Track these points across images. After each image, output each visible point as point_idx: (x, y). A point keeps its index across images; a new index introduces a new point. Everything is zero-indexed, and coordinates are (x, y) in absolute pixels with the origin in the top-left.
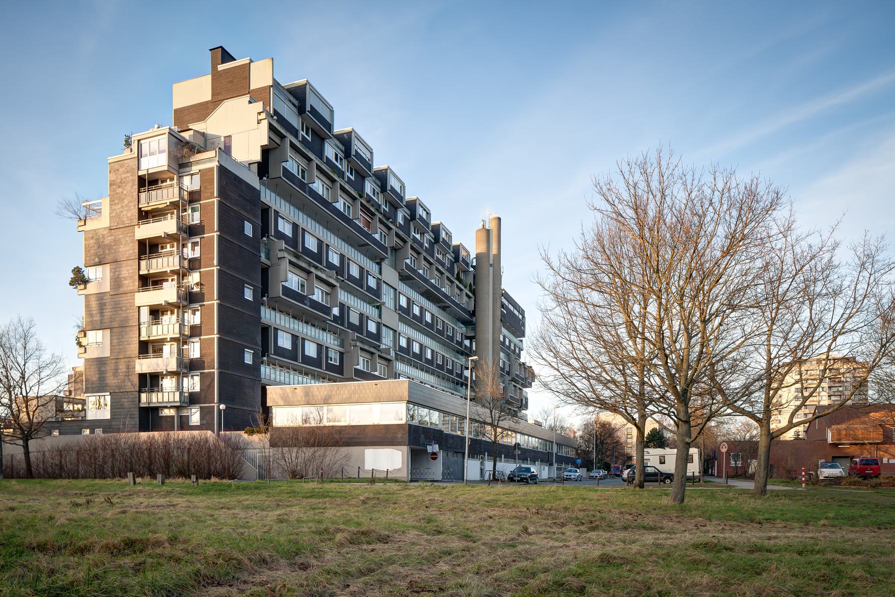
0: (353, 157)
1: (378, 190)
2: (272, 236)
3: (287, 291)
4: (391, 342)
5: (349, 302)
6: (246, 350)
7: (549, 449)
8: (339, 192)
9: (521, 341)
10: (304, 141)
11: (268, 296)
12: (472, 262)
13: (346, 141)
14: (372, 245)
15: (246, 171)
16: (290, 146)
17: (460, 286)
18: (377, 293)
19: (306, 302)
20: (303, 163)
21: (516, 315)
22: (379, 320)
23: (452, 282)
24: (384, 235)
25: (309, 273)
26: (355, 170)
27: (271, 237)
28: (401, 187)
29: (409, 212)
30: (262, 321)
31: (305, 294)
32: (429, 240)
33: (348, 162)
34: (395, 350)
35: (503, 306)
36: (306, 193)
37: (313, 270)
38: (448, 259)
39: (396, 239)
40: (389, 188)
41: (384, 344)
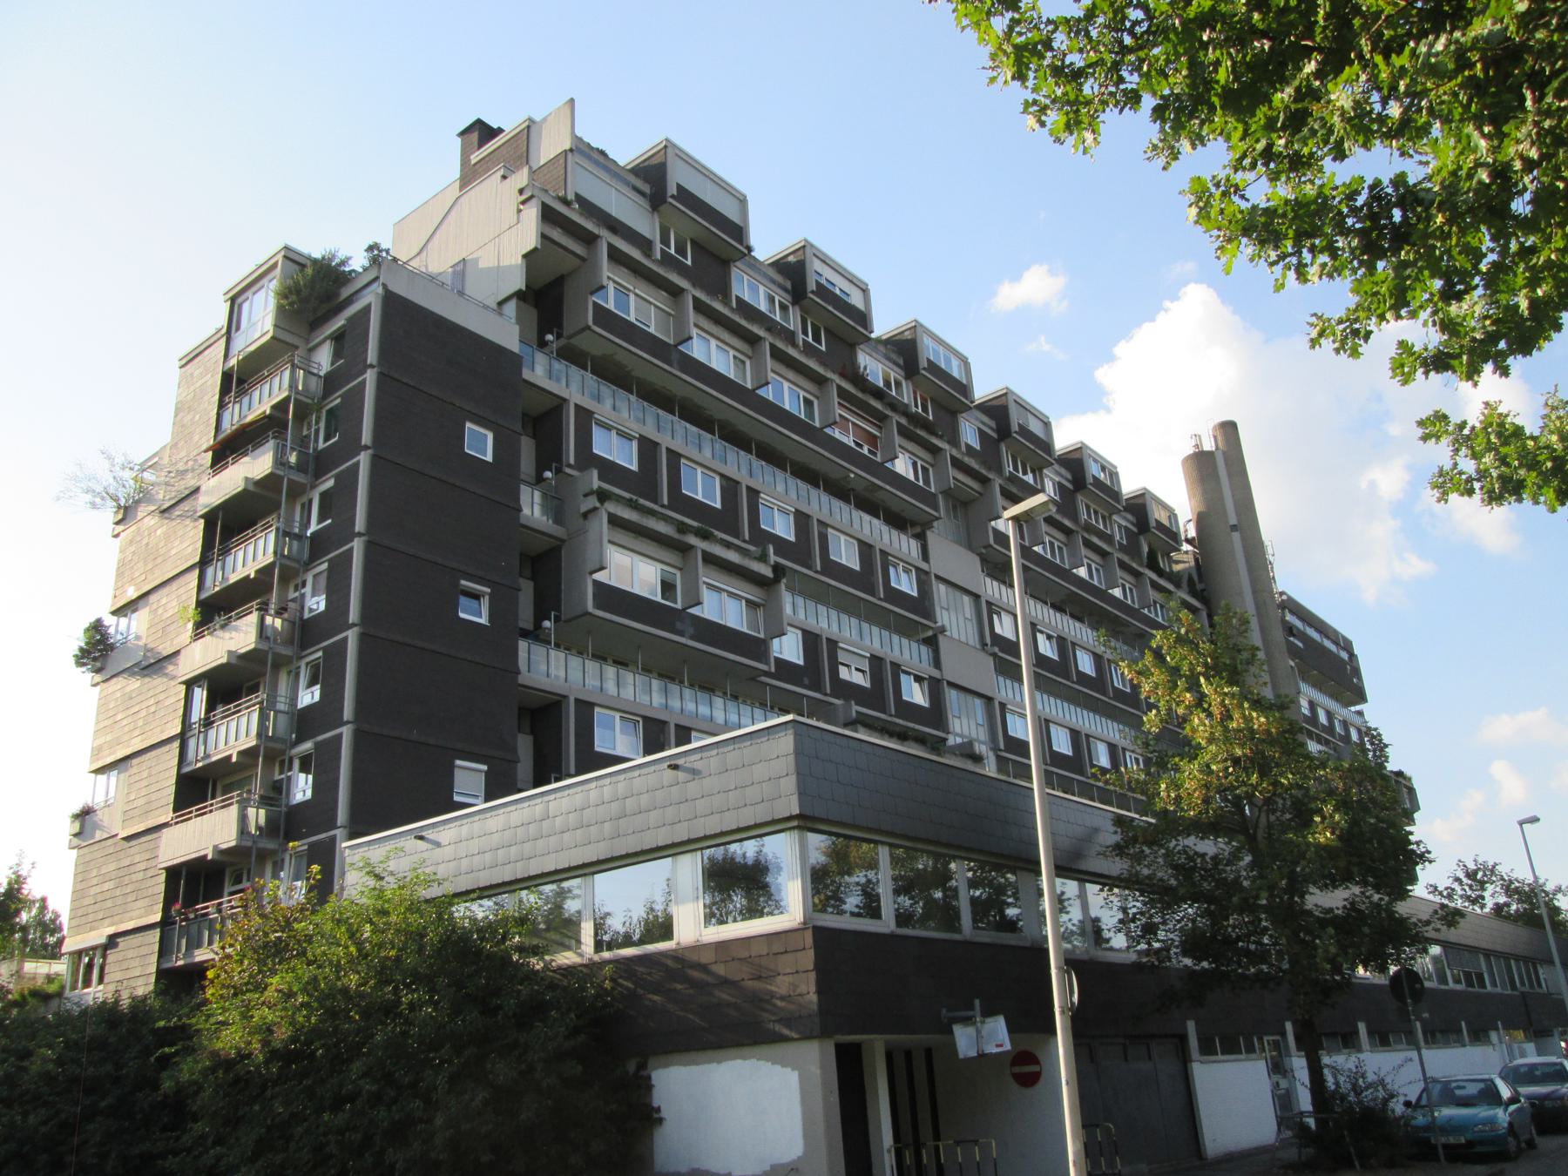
0: (670, 200)
1: (786, 298)
2: (569, 466)
3: (612, 597)
4: (981, 730)
5: (1047, 710)
6: (458, 762)
7: (1523, 984)
8: (692, 315)
9: (1360, 713)
10: (808, 350)
11: (557, 619)
12: (1186, 531)
13: (905, 349)
14: (888, 487)
15: (493, 317)
16: (772, 356)
17: (1162, 582)
18: (922, 605)
19: (679, 625)
20: (658, 299)
21: (1330, 651)
22: (936, 674)
23: (1137, 575)
24: (1097, 569)
25: (684, 550)
26: (932, 400)
27: (568, 470)
28: (1169, 517)
29: (993, 424)
30: (522, 680)
31: (679, 606)
32: (1126, 527)
33: (802, 310)
34: (995, 749)
35: (1290, 630)
36: (671, 365)
37: (692, 540)
38: (1120, 526)
39: (952, 472)
40: (923, 363)
41: (957, 735)
